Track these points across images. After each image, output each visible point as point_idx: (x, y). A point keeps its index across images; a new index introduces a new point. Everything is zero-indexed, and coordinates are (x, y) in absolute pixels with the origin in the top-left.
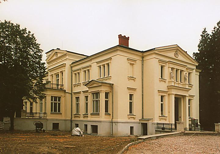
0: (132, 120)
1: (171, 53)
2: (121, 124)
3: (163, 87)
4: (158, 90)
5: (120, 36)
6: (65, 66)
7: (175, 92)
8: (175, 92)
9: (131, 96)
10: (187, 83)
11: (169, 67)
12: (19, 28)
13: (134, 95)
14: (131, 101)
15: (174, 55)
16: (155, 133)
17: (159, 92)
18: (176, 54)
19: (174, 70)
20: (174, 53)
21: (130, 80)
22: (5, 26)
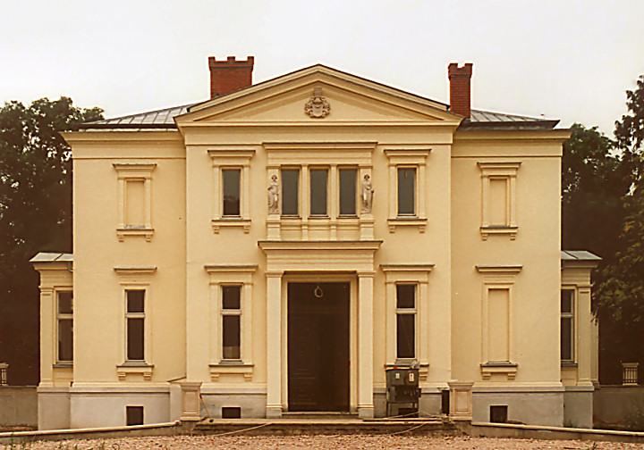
0: (139, 384)
1: (289, 107)
2: (81, 398)
3: (236, 249)
4: (206, 267)
5: (627, 92)
6: (481, 228)
7: (279, 264)
8: (279, 264)
9: (136, 300)
10: (485, 222)
11: (482, 177)
12: (24, 108)
13: (510, 290)
14: (567, 315)
15: (304, 111)
16: (397, 413)
17: (209, 273)
18: (317, 104)
19: (508, 181)
20: (308, 100)
21: (126, 240)
22: (14, 115)
